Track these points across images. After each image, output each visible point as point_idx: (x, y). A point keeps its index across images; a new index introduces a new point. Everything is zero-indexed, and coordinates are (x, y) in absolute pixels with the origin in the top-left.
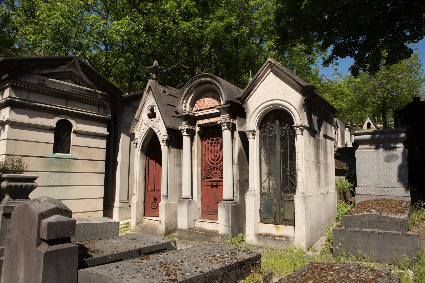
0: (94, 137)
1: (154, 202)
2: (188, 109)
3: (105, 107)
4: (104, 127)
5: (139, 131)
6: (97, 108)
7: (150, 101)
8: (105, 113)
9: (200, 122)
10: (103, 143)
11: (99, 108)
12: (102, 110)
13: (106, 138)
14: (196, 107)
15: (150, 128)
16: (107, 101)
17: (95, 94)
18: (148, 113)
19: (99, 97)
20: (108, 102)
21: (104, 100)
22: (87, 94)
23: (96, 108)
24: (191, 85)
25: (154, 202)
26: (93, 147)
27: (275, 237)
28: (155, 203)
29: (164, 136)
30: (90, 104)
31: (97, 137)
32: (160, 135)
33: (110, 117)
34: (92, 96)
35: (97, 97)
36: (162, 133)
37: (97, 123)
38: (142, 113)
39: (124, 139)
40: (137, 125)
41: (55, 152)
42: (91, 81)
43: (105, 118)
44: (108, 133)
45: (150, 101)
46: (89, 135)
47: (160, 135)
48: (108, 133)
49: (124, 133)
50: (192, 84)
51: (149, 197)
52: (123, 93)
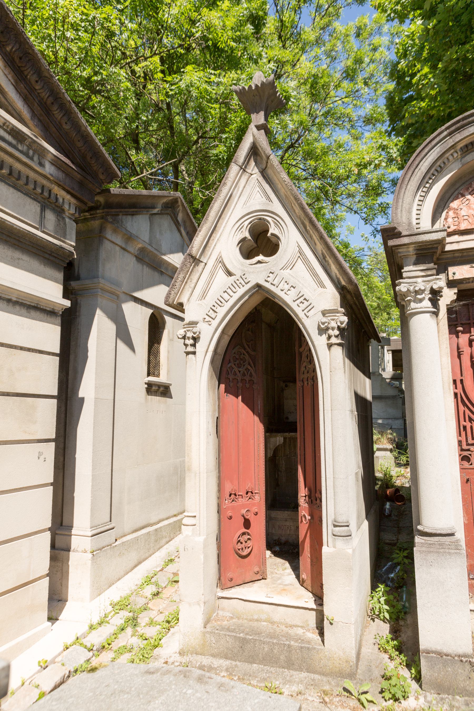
0: (24, 311)
1: (244, 534)
2: (426, 224)
3: (59, 211)
4: (56, 281)
5: (203, 296)
6: (39, 209)
7: (249, 197)
8: (61, 232)
9: (461, 272)
10: (49, 335)
11: (43, 209)
12: (50, 217)
13: (59, 320)
14: (448, 220)
15: (258, 286)
16: (68, 192)
17: (35, 151)
18: (240, 236)
19: (49, 169)
20: (73, 195)
21: (59, 185)
22: (10, 144)
23: (35, 207)
24: (450, 142)
25: (244, 534)
26: (22, 348)
27: (111, 545)
28: (246, 537)
29: (324, 313)
30: (15, 187)
31: (33, 313)
32: (310, 308)
33: (73, 247)
34: (27, 155)
35: (41, 164)
36: (313, 301)
37: (35, 263)
38: (216, 236)
39: (100, 330)
40: (195, 277)
41: (168, 286)
42: (26, 100)
43: (61, 247)
44: (67, 303)
45: (249, 197)
46: (9, 301)
47: (310, 308)
48: (67, 303)
49: (102, 309)
50: (458, 137)
51: (230, 518)
52: (112, 177)
